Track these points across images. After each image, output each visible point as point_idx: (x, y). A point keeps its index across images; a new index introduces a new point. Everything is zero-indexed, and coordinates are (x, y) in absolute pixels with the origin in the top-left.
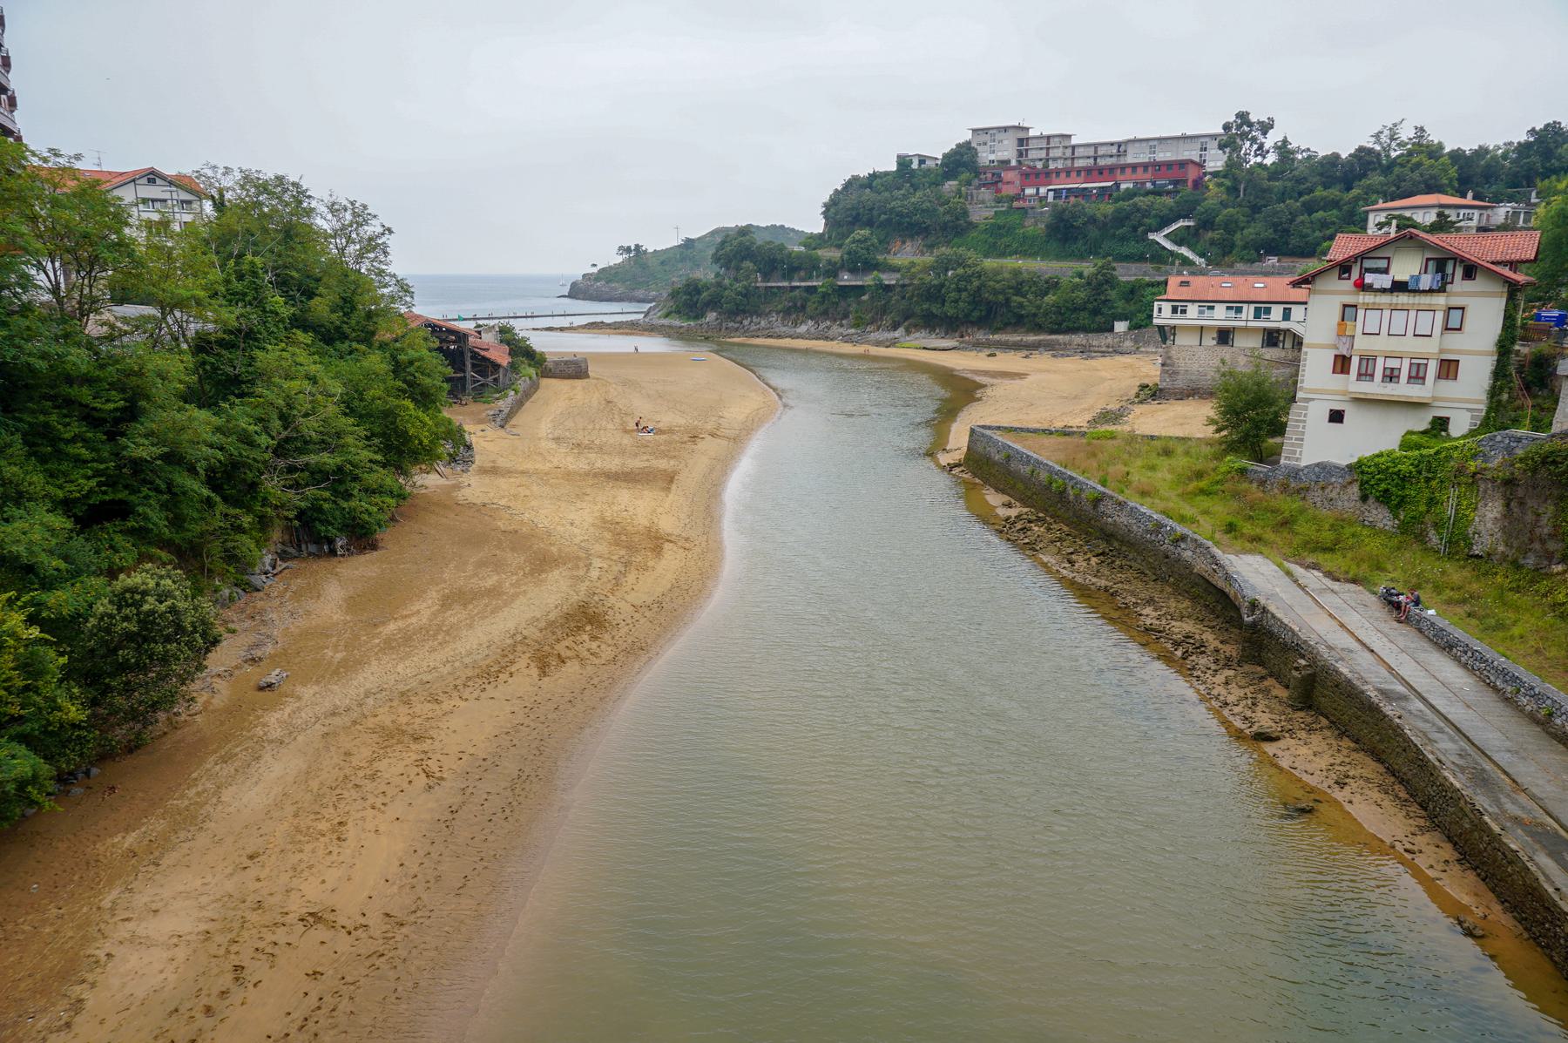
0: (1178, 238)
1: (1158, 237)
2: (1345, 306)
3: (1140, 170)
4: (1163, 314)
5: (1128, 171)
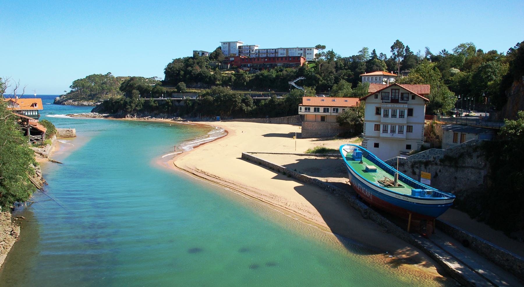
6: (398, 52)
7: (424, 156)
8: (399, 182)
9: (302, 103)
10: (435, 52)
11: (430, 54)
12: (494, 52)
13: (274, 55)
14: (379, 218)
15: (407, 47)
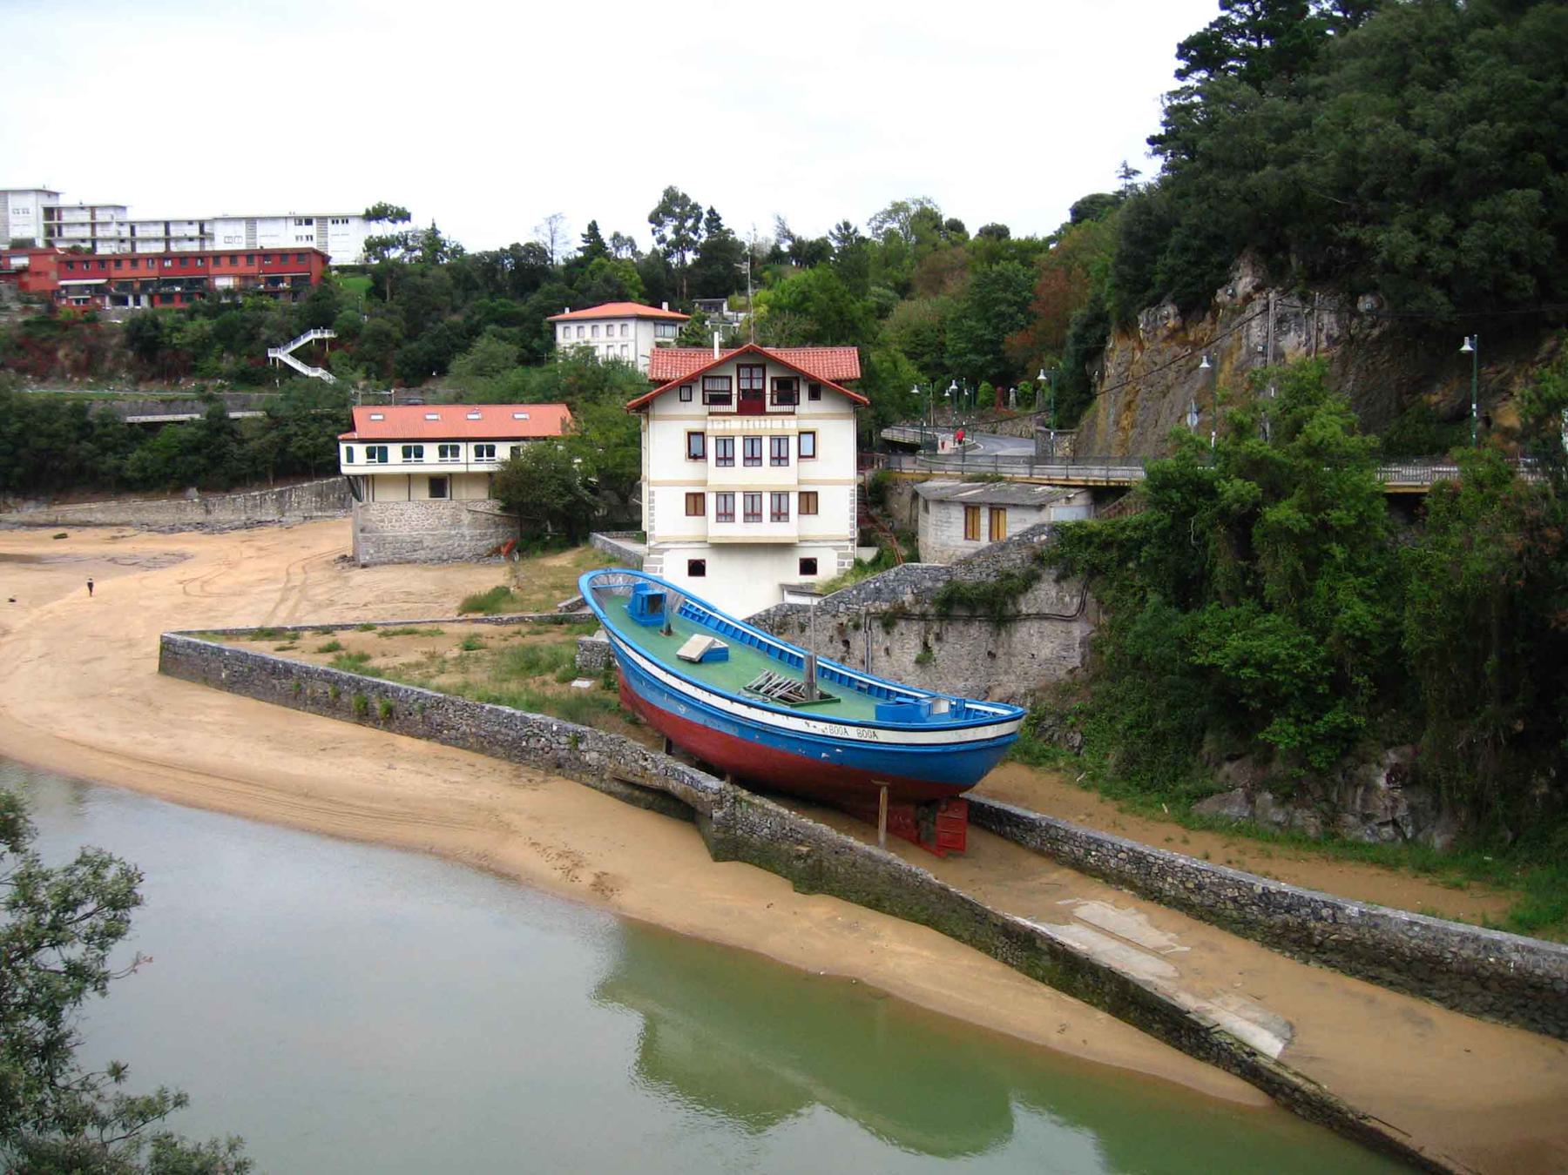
0: (308, 355)
1: (283, 355)
2: (690, 434)
3: (242, 262)
4: (356, 462)
5: (225, 261)
6: (677, 231)
7: (878, 590)
8: (823, 687)
9: (352, 428)
10: (812, 229)
11: (790, 236)
12: (996, 233)
13: (127, 247)
14: (769, 815)
15: (712, 211)
